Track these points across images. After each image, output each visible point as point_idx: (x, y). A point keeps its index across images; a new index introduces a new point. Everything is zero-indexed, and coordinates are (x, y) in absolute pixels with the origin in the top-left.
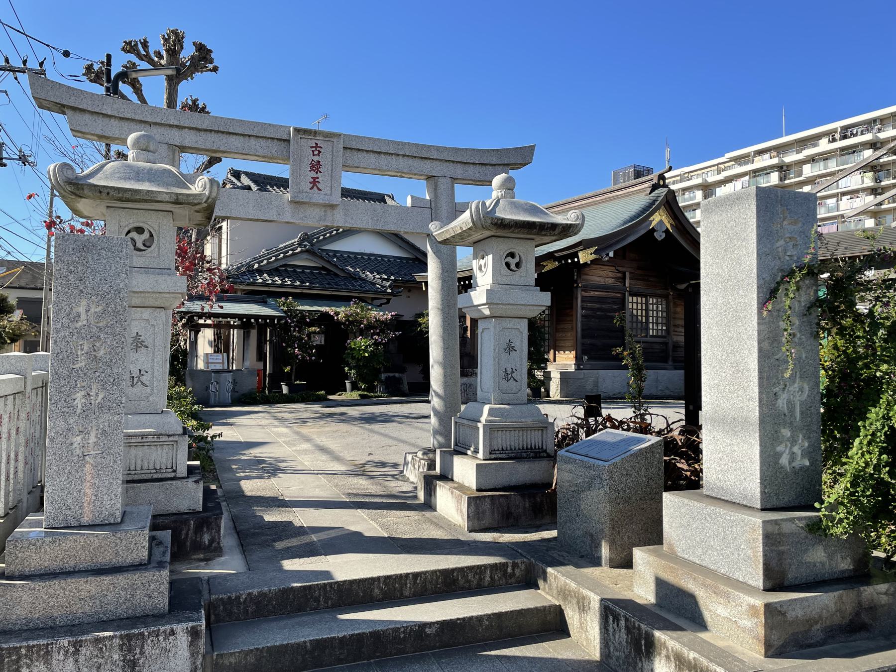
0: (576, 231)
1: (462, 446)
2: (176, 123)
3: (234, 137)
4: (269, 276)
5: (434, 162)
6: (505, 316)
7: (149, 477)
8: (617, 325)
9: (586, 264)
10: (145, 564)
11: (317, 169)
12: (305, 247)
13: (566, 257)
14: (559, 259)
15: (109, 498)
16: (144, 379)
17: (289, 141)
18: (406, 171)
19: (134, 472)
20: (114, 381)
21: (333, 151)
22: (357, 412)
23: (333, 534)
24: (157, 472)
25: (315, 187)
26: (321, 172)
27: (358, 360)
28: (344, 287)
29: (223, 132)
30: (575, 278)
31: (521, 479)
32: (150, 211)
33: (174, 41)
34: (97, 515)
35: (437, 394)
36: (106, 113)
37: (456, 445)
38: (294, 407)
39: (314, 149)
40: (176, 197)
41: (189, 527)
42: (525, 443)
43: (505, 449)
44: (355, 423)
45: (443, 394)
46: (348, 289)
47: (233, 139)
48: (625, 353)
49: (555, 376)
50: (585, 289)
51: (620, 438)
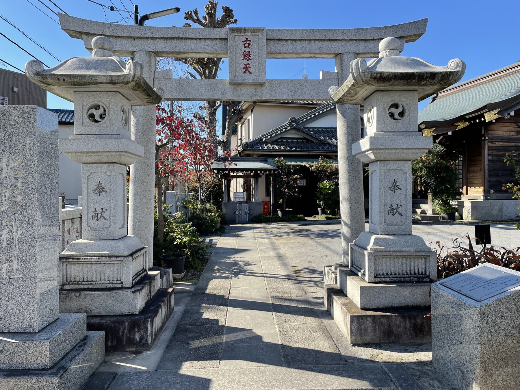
0: (456, 78)
1: (356, 267)
2: (150, 36)
3: (190, 41)
4: (271, 145)
5: (340, 42)
6: (388, 159)
7: (104, 286)
8: (507, 163)
9: (491, 122)
10: (47, 369)
11: (248, 58)
12: (293, 126)
13: (474, 118)
14: (469, 120)
15: (29, 312)
16: (105, 215)
17: (227, 39)
18: (316, 52)
19: (94, 283)
20: (29, 220)
21: (259, 43)
22: (318, 229)
23: (240, 336)
24: (110, 283)
25: (247, 72)
26: (251, 60)
27: (325, 195)
28: (317, 149)
29: (182, 39)
30: (483, 133)
31: (403, 301)
32: (102, 93)
33: (211, 8)
34: (21, 325)
35: (346, 224)
36: (106, 34)
37: (352, 266)
38: (282, 224)
39: (245, 43)
40: (110, 79)
41: (125, 327)
42: (408, 269)
43: (389, 274)
44: (312, 237)
45: (350, 223)
46: (319, 151)
47: (189, 42)
48: (515, 188)
49: (467, 204)
50: (491, 141)
51: (497, 275)
